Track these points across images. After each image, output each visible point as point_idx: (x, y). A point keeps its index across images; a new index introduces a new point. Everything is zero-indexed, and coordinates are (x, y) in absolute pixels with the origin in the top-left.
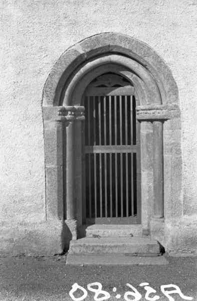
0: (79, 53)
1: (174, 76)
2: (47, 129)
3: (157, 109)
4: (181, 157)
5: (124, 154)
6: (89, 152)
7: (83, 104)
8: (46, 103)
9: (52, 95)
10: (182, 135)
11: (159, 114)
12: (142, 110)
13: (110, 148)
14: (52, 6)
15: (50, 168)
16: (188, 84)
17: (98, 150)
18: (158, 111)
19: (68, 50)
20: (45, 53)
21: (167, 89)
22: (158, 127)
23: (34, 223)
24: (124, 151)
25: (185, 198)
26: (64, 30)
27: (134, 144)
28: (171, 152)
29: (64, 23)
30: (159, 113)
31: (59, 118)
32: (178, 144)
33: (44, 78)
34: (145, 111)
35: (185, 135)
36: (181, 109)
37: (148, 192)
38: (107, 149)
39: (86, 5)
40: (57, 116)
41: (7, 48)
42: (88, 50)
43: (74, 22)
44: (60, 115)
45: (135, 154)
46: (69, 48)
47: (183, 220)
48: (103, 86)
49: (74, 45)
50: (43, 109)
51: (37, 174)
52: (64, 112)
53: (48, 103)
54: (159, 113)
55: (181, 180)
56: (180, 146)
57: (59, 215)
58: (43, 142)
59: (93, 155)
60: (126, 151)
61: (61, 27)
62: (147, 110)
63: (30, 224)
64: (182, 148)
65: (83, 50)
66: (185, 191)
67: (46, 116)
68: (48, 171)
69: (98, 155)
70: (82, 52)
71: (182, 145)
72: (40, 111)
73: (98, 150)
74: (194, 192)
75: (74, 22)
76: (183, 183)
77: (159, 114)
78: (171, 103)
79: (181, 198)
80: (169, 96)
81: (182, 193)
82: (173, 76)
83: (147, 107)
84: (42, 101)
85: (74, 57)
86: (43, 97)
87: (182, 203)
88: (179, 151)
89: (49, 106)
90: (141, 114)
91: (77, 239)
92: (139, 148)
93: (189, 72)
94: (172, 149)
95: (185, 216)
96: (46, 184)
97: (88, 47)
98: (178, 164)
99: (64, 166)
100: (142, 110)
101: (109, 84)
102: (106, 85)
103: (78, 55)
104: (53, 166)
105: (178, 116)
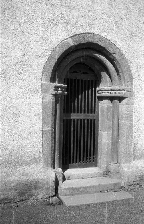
0: (70, 45)
1: (131, 69)
2: (44, 100)
3: (118, 90)
4: (133, 123)
5: (88, 120)
6: (68, 118)
7: (66, 82)
8: (45, 80)
9: (49, 75)
10: (134, 109)
11: (118, 94)
12: (106, 90)
13: (79, 115)
14: (52, 7)
15: (46, 130)
16: (139, 75)
17: (74, 116)
18: (118, 92)
19: (63, 42)
20: (45, 42)
21: (126, 77)
22: (117, 102)
23: (33, 174)
24: (88, 118)
25: (134, 150)
26: (60, 26)
27: (95, 113)
28: (127, 119)
29: (61, 21)
30: (119, 93)
31: (54, 92)
32: (131, 115)
33: (43, 61)
34: (108, 92)
35: (136, 109)
36: (134, 91)
37: (107, 146)
38: (78, 116)
39: (77, 10)
40: (53, 90)
41: (15, 34)
42: (77, 43)
43: (68, 21)
44: (54, 90)
45: (95, 120)
46: (64, 40)
47: (133, 165)
48: (76, 72)
49: (67, 39)
50: (42, 84)
51: (36, 135)
52: (56, 88)
53: (46, 80)
54: (119, 93)
55: (132, 138)
56: (133, 116)
57: (51, 166)
58: (41, 111)
59: (71, 120)
60: (82, 117)
61: (58, 23)
62: (109, 91)
63: (30, 175)
64: (133, 117)
65: (74, 44)
66: (134, 145)
67: (45, 90)
68: (44, 133)
69: (74, 120)
70: (72, 44)
71: (133, 115)
72: (40, 86)
73: (74, 116)
74: (139, 146)
75: (68, 21)
76: (134, 140)
77: (119, 94)
78: (128, 87)
79: (132, 150)
80: (127, 81)
81: (133, 147)
82: (131, 68)
83: (110, 88)
84: (42, 78)
85: (66, 48)
86: (42, 75)
87: (132, 153)
88: (132, 119)
89: (47, 83)
90: (104, 93)
91: (63, 182)
92: (98, 115)
93: (140, 67)
94: (127, 118)
95: (134, 161)
96: (42, 142)
97: (77, 41)
98: (131, 128)
99: (55, 128)
100: (106, 90)
101: (80, 71)
102: (78, 71)
103: (70, 46)
104: (49, 129)
105: (132, 96)
